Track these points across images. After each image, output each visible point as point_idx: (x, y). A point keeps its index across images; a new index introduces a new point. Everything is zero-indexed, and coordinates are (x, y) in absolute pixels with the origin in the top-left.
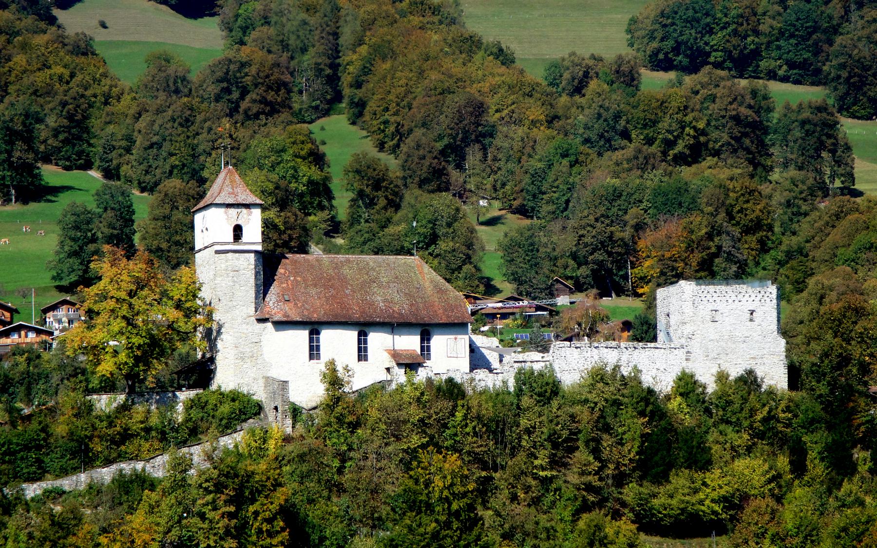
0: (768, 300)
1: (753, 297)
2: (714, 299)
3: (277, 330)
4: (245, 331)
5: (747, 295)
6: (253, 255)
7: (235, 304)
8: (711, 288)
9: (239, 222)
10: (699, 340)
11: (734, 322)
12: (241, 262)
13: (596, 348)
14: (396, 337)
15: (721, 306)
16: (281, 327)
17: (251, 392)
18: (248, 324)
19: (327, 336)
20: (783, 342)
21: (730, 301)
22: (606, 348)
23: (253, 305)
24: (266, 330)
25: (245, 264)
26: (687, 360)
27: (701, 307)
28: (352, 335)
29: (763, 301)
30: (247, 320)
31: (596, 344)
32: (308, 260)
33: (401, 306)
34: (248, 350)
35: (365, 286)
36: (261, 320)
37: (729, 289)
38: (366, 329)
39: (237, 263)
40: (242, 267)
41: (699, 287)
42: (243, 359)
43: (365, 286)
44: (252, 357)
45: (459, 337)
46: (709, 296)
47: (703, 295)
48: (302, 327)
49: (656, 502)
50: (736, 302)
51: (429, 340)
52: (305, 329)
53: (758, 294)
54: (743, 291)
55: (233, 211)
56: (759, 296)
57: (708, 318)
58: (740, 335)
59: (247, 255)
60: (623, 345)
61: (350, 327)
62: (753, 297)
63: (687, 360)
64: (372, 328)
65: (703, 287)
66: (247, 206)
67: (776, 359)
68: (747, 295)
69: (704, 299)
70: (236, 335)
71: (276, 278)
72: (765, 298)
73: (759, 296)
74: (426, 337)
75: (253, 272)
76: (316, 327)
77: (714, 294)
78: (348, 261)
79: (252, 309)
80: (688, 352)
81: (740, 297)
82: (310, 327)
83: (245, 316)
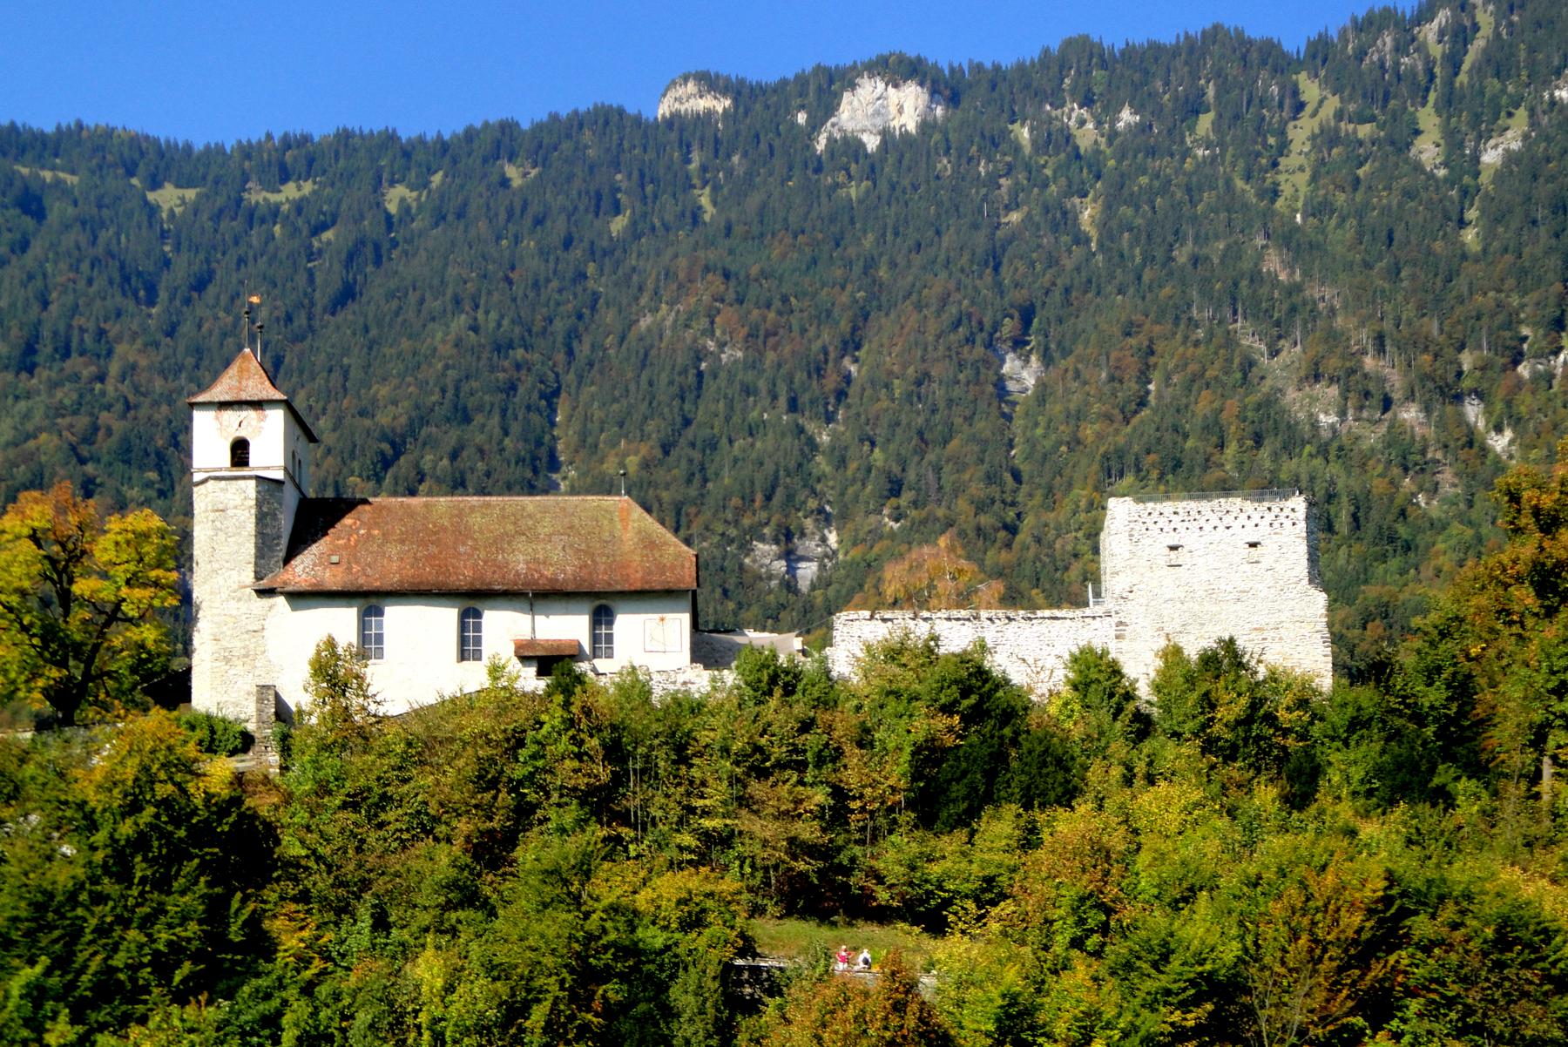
0: (1288, 523)
1: (1256, 518)
2: (1173, 525)
3: (294, 609)
4: (235, 613)
5: (1243, 516)
6: (253, 483)
7: (216, 566)
8: (1168, 507)
9: (243, 433)
10: (1143, 601)
11: (1216, 565)
12: (229, 495)
13: (925, 619)
14: (540, 619)
15: (1188, 539)
16: (301, 602)
17: (242, 716)
18: (240, 600)
19: (396, 617)
20: (1321, 599)
21: (1208, 527)
22: (949, 619)
23: (251, 568)
24: (274, 611)
25: (238, 500)
26: (1117, 637)
27: (1146, 541)
28: (446, 617)
29: (1276, 524)
30: (239, 594)
31: (925, 614)
32: (409, 506)
33: (560, 565)
34: (239, 644)
35: (500, 542)
36: (264, 593)
37: (1204, 506)
38: (478, 605)
39: (222, 497)
40: (231, 504)
41: (1141, 506)
42: (227, 660)
43: (500, 542)
44: (246, 656)
45: (668, 616)
46: (1162, 522)
47: (1150, 521)
48: (344, 602)
49: (935, 870)
50: (1221, 528)
51: (610, 623)
52: (351, 606)
53: (1266, 514)
54: (1235, 510)
55: (230, 416)
56: (1269, 517)
57: (1162, 561)
58: (1229, 589)
59: (241, 483)
60: (984, 614)
61: (443, 600)
62: (1256, 518)
63: (1117, 637)
64: (489, 603)
65: (1150, 505)
66: (258, 405)
67: (1307, 629)
68: (1243, 516)
69: (1151, 526)
70: (216, 619)
71: (331, 531)
72: (1282, 519)
73: (1269, 517)
74: (602, 616)
75: (253, 511)
76: (373, 601)
77: (1173, 517)
78: (488, 505)
79: (249, 576)
80: (1120, 623)
81: (1228, 520)
82: (361, 601)
83: (235, 586)
